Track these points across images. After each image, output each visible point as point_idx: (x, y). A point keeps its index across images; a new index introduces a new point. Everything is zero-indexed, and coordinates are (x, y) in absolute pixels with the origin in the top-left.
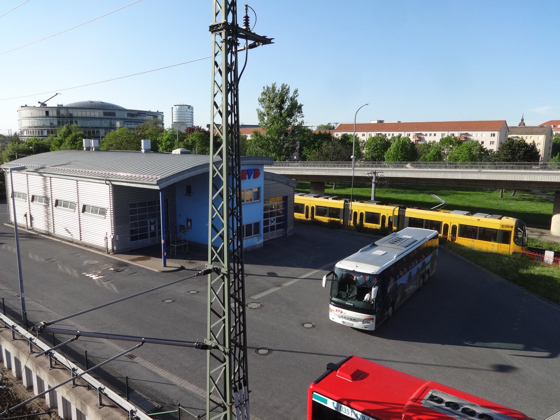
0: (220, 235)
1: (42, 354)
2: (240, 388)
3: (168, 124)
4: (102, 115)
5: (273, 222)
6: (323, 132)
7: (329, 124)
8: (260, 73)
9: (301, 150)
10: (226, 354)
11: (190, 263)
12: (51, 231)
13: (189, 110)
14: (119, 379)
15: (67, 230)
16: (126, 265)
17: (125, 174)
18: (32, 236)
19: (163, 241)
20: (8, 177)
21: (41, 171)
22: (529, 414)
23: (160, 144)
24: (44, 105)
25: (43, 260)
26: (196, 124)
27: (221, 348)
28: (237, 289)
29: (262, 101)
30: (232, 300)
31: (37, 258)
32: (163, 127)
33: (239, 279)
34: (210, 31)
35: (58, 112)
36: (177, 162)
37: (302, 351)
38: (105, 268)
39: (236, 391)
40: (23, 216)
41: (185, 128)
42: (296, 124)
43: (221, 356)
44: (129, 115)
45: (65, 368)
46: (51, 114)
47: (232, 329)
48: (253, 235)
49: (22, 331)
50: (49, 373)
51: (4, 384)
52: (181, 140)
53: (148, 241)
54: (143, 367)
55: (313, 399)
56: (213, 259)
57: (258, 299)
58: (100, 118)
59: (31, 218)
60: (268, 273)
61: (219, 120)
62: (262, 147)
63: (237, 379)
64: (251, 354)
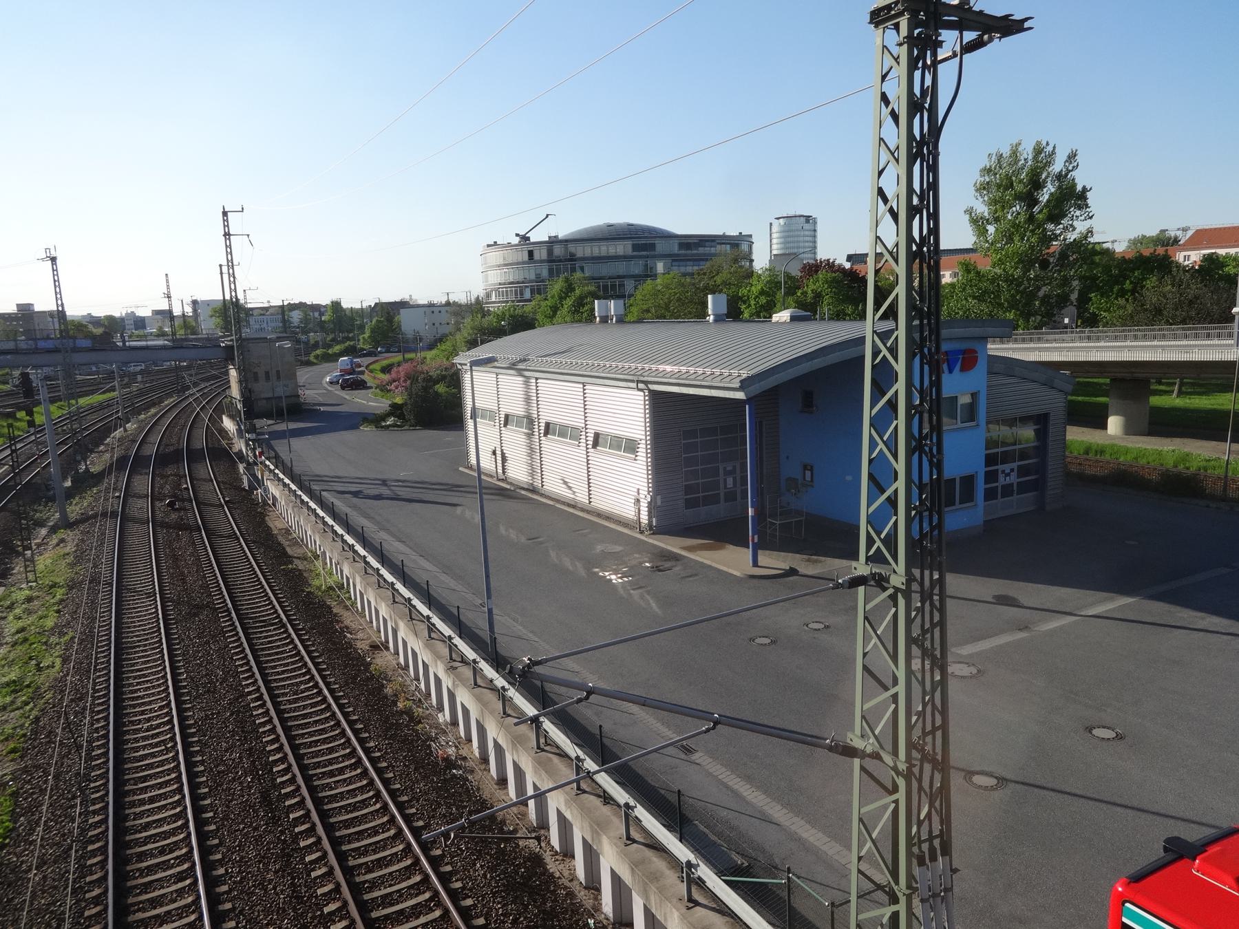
0: (889, 499)
1: (525, 722)
2: (933, 859)
3: (761, 260)
4: (629, 251)
5: (1008, 475)
6: (1146, 253)
7: (1163, 231)
8: (994, 109)
9: (1083, 300)
10: (898, 773)
11: (808, 560)
12: (538, 484)
13: (807, 226)
14: (663, 792)
15: (565, 483)
16: (676, 558)
17: (676, 369)
18: (505, 492)
19: (751, 512)
20: (467, 378)
21: (521, 366)
23: (744, 302)
24: (525, 238)
25: (523, 539)
26: (823, 254)
27: (888, 759)
28: (927, 626)
29: (983, 188)
30: (916, 651)
31: (513, 535)
32: (751, 266)
33: (932, 604)
34: (871, 22)
35: (550, 252)
36: (786, 338)
37: (1089, 795)
38: (634, 562)
39: (921, 863)
40: (490, 454)
41: (800, 266)
42: (1072, 237)
43: (886, 776)
44: (681, 246)
45: (563, 755)
46: (537, 256)
47: (914, 719)
48: (958, 506)
49: (488, 671)
50: (534, 759)
51: (460, 767)
52: (791, 291)
53: (721, 510)
54: (710, 774)
55: (1124, 920)
56: (871, 553)
57: (971, 656)
58: (625, 258)
59: (504, 459)
60: (995, 597)
61: (890, 233)
62: (980, 299)
63: (924, 836)
64: (956, 780)
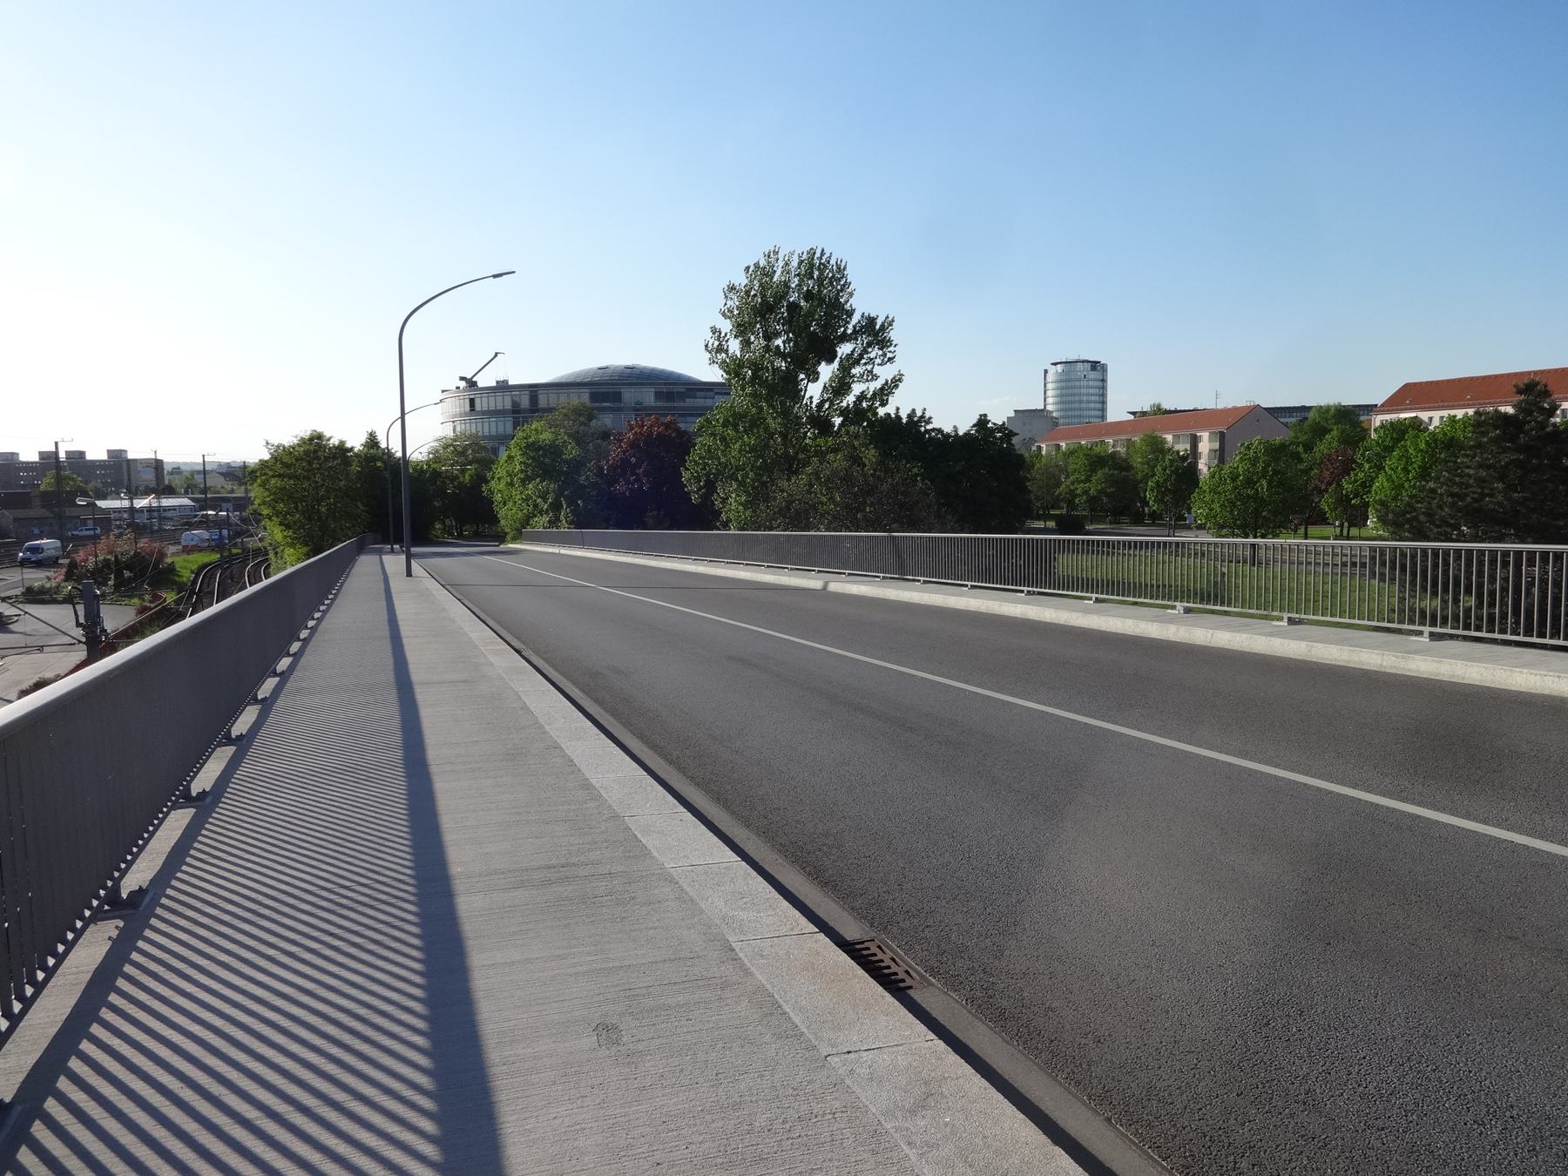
13: (1093, 375)
22: (1115, 1167)
